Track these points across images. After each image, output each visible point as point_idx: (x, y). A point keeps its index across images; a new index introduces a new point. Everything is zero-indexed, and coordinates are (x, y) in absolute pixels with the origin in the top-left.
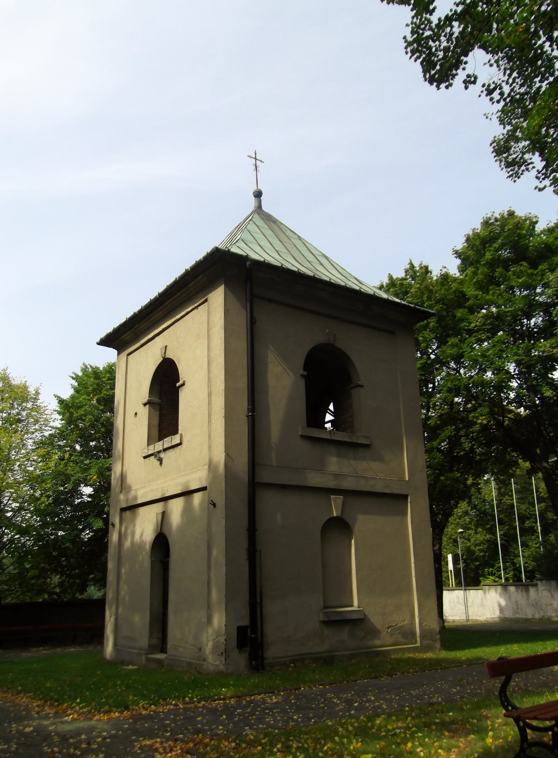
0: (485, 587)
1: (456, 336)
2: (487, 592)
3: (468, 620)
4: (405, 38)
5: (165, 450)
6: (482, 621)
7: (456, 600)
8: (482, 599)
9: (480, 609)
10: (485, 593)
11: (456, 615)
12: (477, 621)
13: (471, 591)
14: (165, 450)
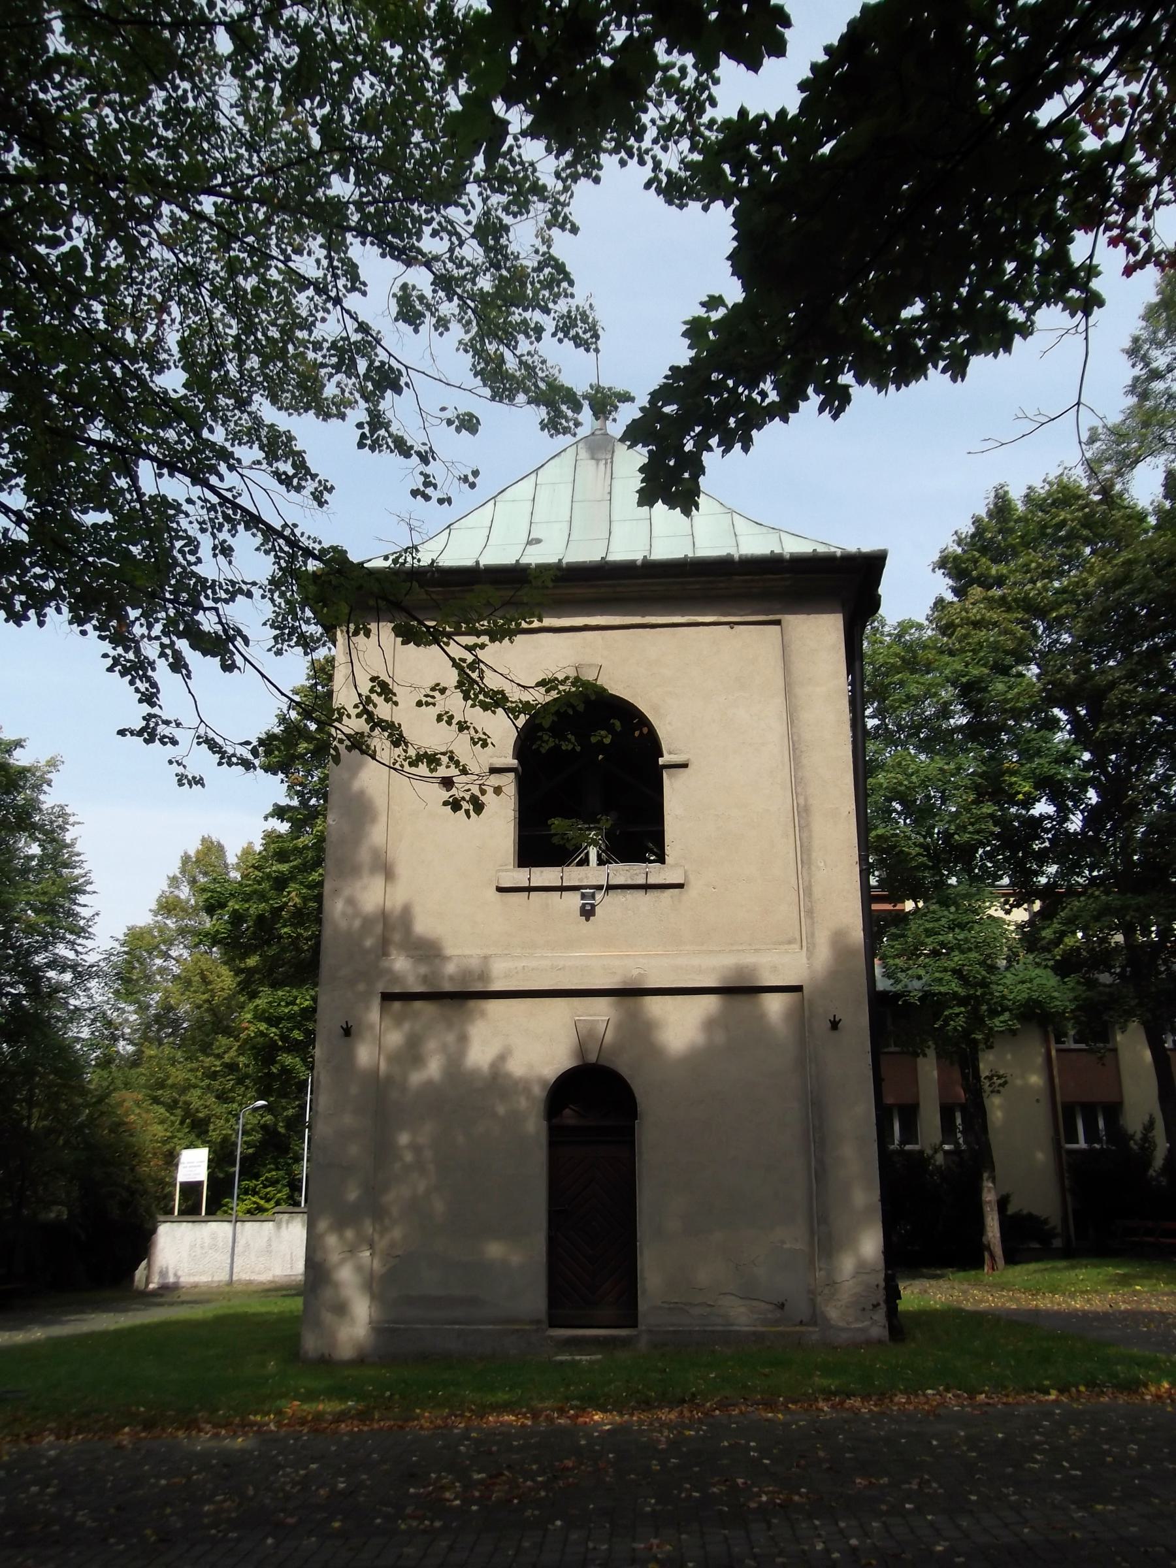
0: (281, 1216)
1: (743, 128)
2: (284, 1225)
3: (230, 1282)
4: (49, 785)
5: (611, 888)
6: (262, 1283)
7: (207, 1241)
8: (270, 1240)
9: (261, 1259)
10: (279, 1227)
11: (203, 1273)
12: (250, 1282)
13: (248, 1224)
14: (611, 888)
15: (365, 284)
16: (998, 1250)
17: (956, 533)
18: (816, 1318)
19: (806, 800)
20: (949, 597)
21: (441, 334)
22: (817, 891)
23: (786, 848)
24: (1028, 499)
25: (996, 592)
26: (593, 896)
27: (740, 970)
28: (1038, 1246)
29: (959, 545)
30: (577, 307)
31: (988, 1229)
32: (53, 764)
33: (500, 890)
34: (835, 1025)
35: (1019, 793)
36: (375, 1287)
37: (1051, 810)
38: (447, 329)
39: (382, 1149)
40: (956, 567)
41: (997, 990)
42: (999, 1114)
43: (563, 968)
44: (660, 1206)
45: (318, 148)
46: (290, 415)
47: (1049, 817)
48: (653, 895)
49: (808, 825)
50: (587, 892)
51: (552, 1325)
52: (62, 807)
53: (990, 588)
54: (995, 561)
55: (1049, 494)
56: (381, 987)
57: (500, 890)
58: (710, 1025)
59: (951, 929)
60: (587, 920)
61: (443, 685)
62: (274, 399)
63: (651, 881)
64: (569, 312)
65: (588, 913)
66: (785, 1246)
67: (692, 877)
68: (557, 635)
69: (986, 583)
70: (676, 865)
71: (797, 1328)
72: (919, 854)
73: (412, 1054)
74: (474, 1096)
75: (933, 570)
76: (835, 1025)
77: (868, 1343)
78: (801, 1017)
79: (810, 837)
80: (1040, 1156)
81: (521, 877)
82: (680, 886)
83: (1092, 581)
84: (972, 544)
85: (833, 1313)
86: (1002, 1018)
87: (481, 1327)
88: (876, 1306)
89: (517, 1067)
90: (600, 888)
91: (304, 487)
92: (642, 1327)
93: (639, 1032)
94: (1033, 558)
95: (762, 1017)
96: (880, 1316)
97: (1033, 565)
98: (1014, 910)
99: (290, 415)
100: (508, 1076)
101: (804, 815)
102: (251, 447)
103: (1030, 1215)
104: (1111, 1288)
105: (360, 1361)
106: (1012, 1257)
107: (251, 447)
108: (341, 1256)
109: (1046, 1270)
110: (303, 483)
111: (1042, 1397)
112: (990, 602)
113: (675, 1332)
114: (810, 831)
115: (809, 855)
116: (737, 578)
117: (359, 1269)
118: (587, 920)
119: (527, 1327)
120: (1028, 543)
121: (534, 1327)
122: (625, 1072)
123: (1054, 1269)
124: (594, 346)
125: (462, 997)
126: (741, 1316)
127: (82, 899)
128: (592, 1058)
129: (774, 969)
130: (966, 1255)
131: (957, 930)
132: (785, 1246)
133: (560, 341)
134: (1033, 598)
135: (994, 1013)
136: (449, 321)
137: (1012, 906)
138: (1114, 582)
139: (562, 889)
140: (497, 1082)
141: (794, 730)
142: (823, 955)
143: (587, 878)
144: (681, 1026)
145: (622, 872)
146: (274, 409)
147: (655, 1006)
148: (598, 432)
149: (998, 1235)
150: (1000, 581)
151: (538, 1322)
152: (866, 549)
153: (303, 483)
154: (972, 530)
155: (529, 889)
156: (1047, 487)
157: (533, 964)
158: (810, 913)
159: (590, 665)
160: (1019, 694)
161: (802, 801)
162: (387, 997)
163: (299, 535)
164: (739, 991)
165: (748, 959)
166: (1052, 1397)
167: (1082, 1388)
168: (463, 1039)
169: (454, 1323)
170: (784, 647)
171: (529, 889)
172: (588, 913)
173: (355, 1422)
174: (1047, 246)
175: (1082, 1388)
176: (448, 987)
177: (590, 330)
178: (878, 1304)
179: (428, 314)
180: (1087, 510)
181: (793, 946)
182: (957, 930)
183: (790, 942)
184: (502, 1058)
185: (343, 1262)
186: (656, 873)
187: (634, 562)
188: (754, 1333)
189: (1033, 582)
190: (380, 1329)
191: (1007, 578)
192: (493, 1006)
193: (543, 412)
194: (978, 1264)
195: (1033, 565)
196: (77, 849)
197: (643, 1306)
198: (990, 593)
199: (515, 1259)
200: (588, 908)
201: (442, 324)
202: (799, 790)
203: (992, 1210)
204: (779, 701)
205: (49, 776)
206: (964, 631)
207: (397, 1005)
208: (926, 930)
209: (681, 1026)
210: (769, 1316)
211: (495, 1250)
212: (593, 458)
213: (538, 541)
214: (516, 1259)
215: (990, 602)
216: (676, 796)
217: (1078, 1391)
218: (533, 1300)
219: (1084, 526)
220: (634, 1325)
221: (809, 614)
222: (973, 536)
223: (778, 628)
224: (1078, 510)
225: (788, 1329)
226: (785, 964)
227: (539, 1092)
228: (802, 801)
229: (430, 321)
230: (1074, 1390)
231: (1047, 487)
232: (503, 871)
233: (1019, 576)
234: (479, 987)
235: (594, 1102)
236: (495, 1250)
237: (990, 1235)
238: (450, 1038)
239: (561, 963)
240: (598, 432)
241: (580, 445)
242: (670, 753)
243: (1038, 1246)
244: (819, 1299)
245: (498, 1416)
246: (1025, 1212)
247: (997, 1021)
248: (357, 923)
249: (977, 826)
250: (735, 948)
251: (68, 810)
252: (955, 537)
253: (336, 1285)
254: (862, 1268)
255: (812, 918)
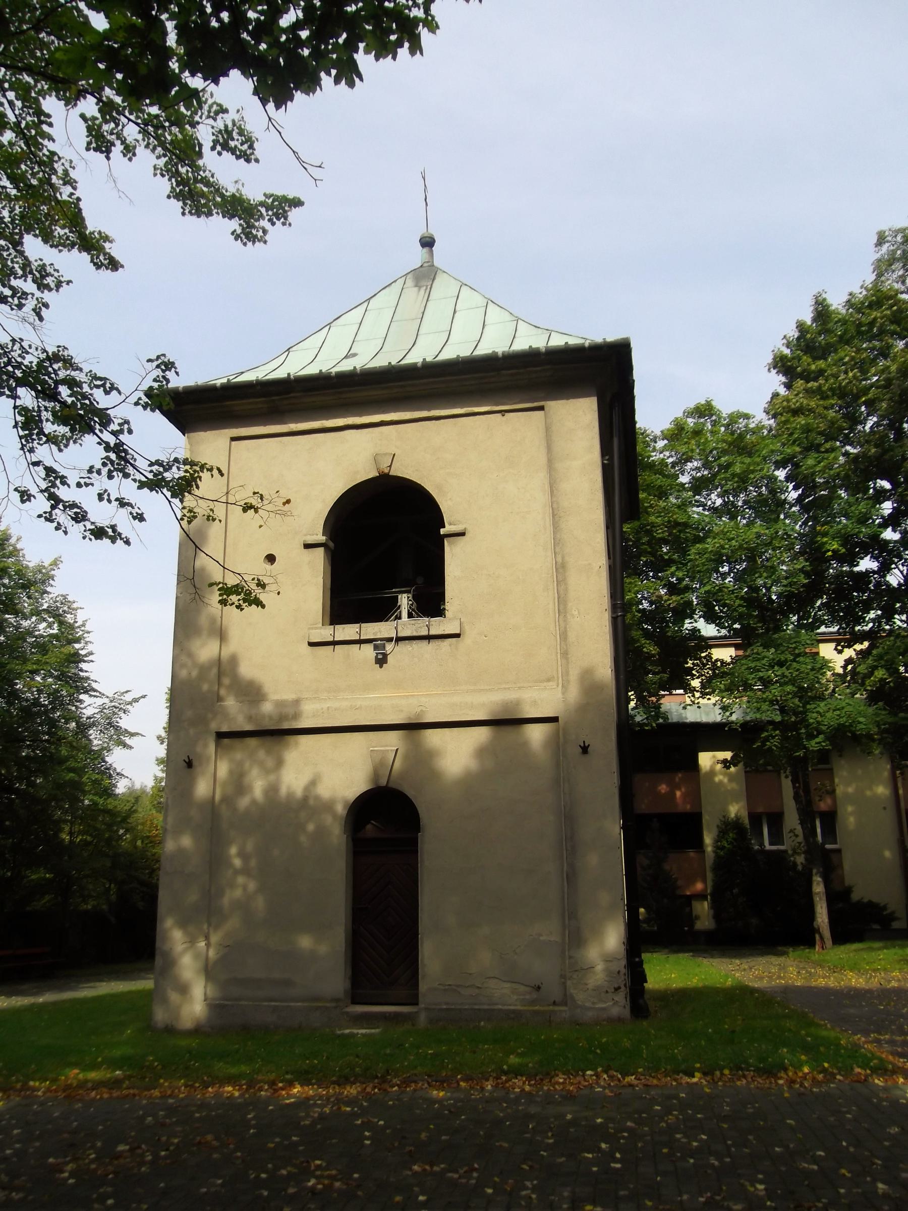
5: (399, 639)
14: (399, 639)
15: (49, 116)
16: (826, 933)
17: (785, 337)
18: (566, 1000)
19: (563, 558)
20: (782, 391)
21: (130, 159)
22: (572, 636)
23: (548, 600)
24: (849, 304)
25: (812, 384)
26: (384, 647)
27: (506, 706)
28: (878, 927)
29: (788, 347)
30: (233, 121)
31: (818, 915)
32: (55, 563)
33: (311, 644)
34: (585, 749)
35: (829, 551)
36: (208, 971)
37: (874, 565)
38: (134, 154)
40: (783, 366)
41: (812, 718)
42: (852, 819)
43: (360, 708)
44: (437, 903)
45: (107, 26)
46: (60, 251)
47: (874, 572)
48: (434, 644)
49: (564, 580)
50: (378, 644)
51: (355, 1002)
52: (65, 597)
53: (808, 382)
54: (815, 359)
55: (866, 297)
56: (214, 726)
57: (311, 644)
58: (481, 752)
59: (771, 666)
60: (381, 667)
62: (47, 237)
63: (432, 632)
64: (226, 126)
65: (381, 661)
66: (542, 938)
67: (467, 627)
68: (359, 431)
69: (807, 376)
70: (455, 618)
71: (551, 1008)
72: (740, 605)
74: (285, 816)
75: (769, 370)
76: (585, 749)
77: (611, 1020)
78: (557, 744)
79: (566, 590)
80: (887, 854)
81: (327, 633)
82: (457, 636)
83: (893, 368)
84: (798, 346)
85: (580, 997)
86: (817, 740)
87: (292, 1004)
88: (617, 989)
89: (324, 791)
90: (390, 640)
91: (24, 305)
92: (422, 1005)
93: (421, 760)
94: (847, 353)
95: (525, 744)
96: (621, 998)
97: (847, 359)
98: (845, 650)
99: (60, 251)
100: (317, 798)
101: (561, 570)
102: (25, 281)
103: (870, 902)
104: (898, 967)
105: (196, 1031)
106: (841, 936)
107: (25, 281)
108: (184, 946)
109: (862, 949)
110: (23, 301)
111: (686, 1079)
112: (809, 392)
113: (447, 1009)
114: (566, 584)
115: (565, 605)
116: (504, 372)
117: (197, 956)
118: (381, 667)
119: (328, 1005)
120: (845, 340)
121: (333, 1004)
122: (410, 793)
123: (871, 949)
124: (253, 157)
125: (277, 734)
126: (506, 995)
127: (83, 666)
128: (383, 782)
129: (534, 703)
130: (795, 934)
131: (776, 668)
132: (542, 938)
133: (220, 154)
134: (845, 387)
135: (811, 737)
136: (135, 147)
137: (843, 647)
139: (360, 642)
140: (308, 804)
141: (554, 499)
142: (574, 694)
143: (380, 632)
144: (456, 754)
145: (420, 626)
146: (47, 247)
147: (433, 737)
148: (426, 265)
149: (826, 920)
150: (821, 372)
151: (337, 1000)
152: (610, 338)
153: (23, 301)
154: (797, 335)
155: (334, 643)
156: (864, 293)
157: (336, 704)
158: (565, 654)
159: (385, 454)
160: (825, 467)
161: (559, 560)
163: (27, 347)
164: (506, 723)
166: (695, 1080)
167: (726, 1072)
169: (271, 1000)
170: (548, 429)
171: (334, 643)
172: (381, 661)
173: (104, 1090)
175: (726, 1072)
177: (246, 142)
178: (619, 988)
179: (118, 143)
180: (895, 308)
181: (551, 683)
182: (776, 668)
183: (548, 680)
184: (313, 783)
185: (185, 951)
186: (438, 626)
187: (416, 364)
188: (514, 1011)
189: (846, 373)
190: (216, 1007)
191: (826, 371)
192: (304, 739)
193: (235, 224)
194: (811, 944)
195: (847, 359)
196: (87, 628)
197: (423, 987)
198: (810, 385)
199: (321, 949)
200: (380, 657)
201: (129, 151)
202: (557, 550)
203: (820, 899)
204: (540, 478)
205: (53, 572)
206: (783, 419)
207: (226, 741)
208: (749, 668)
209: (456, 754)
210: (528, 997)
211: (305, 942)
212: (416, 286)
213: (355, 355)
214: (323, 949)
215: (809, 392)
216: (456, 562)
217: (722, 1074)
218: (335, 981)
219: (892, 322)
220: (416, 1003)
221: (568, 399)
222: (798, 339)
223: (542, 413)
224: (887, 309)
225: (542, 1008)
226: (544, 698)
227: (341, 809)
228: (559, 560)
229: (118, 148)
230: (718, 1073)
231: (864, 293)
232: (312, 628)
233: (835, 369)
234: (286, 726)
235: (386, 818)
236: (305, 942)
237: (819, 920)
239: (359, 703)
240: (426, 265)
241: (409, 276)
242: (450, 524)
243: (878, 927)
244: (569, 983)
245: (220, 1087)
246: (865, 900)
247: (813, 743)
248: (194, 673)
249: (790, 580)
250: (504, 686)
251: (70, 598)
252: (785, 341)
254: (608, 959)
255: (567, 659)
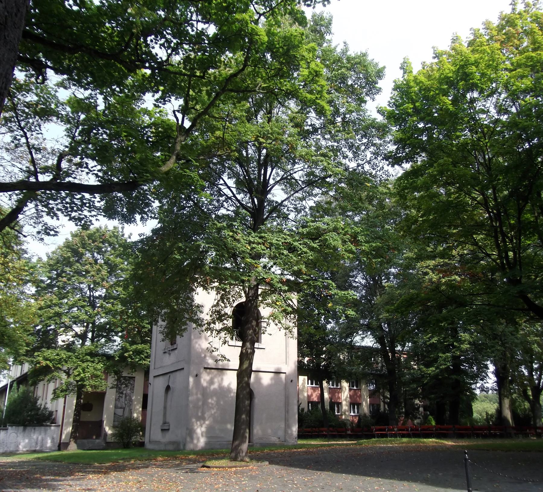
27: (279, 369)
39: (205, 403)
58: (272, 379)
61: (167, 355)
73: (211, 382)
95: (281, 378)
138: (21, 480)
162: (205, 368)
164: (277, 373)
165: (280, 366)
168: (222, 379)
174: (504, 120)
176: (220, 367)
184: (230, 384)
190: (207, 443)
207: (208, 370)
238: (220, 379)
253: (196, 434)
